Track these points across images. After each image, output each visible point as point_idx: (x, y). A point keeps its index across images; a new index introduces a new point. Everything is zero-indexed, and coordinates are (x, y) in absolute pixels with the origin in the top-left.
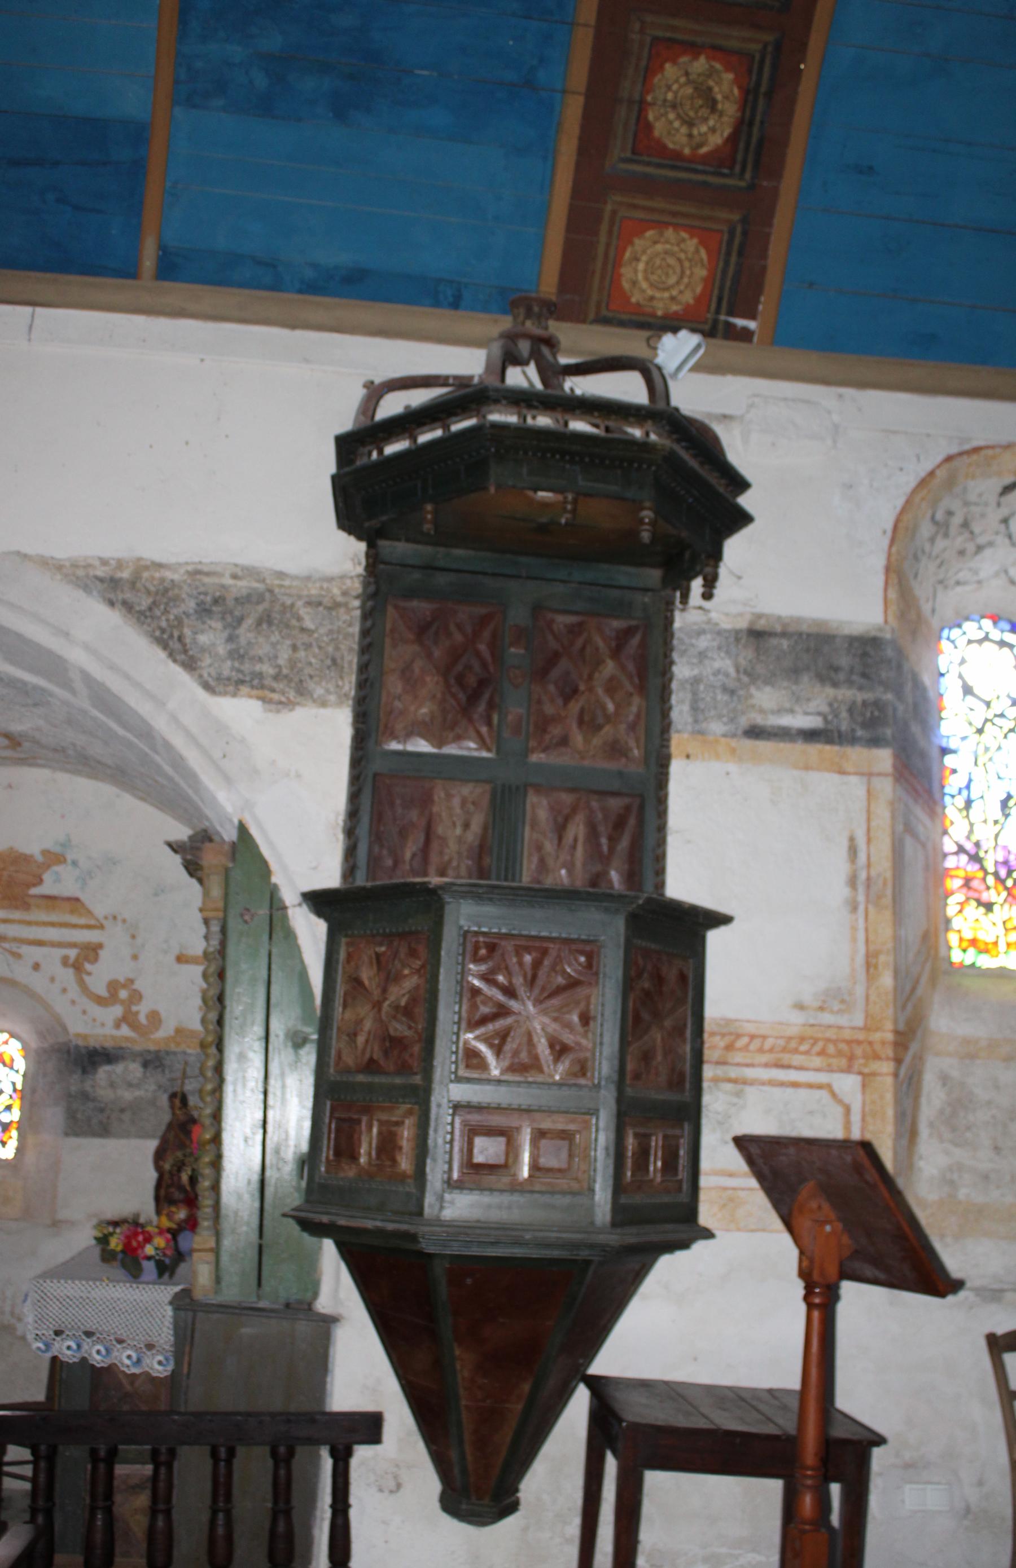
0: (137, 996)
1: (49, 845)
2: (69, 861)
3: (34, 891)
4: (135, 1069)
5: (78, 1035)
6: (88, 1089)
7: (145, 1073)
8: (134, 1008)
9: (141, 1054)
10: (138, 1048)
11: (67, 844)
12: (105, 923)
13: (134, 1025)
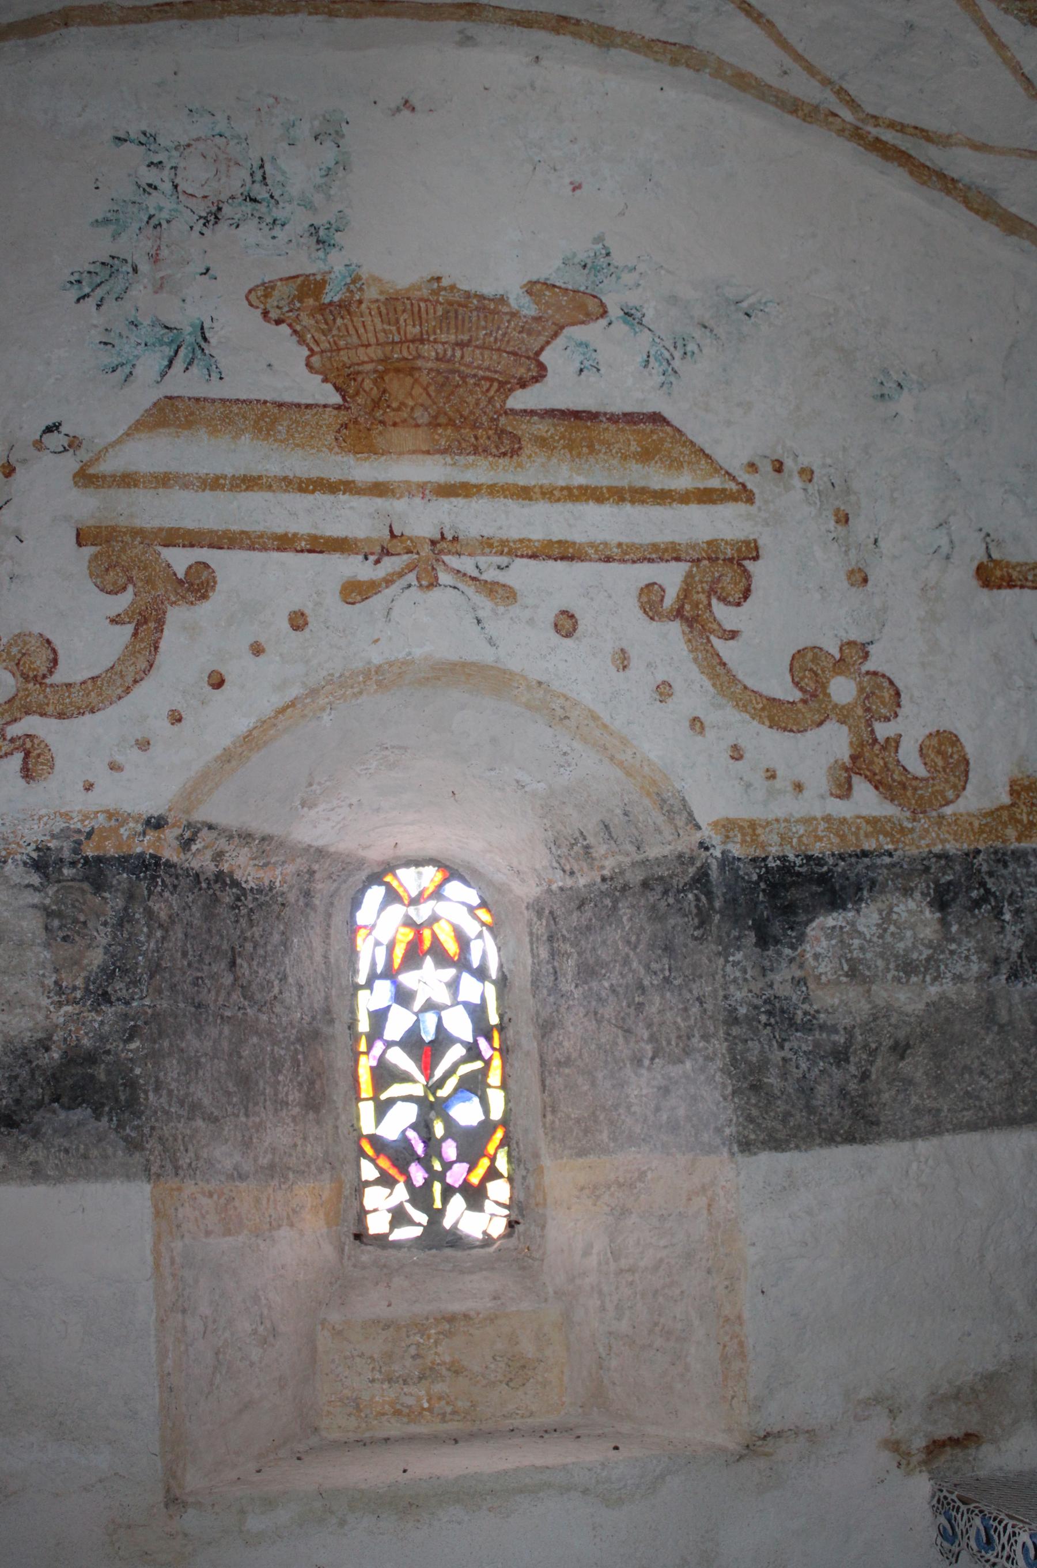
0: (883, 695)
1: (548, 268)
2: (614, 312)
3: (520, 400)
4: (914, 916)
5: (727, 827)
6: (783, 990)
7: (944, 923)
8: (883, 730)
9: (922, 866)
10: (913, 848)
11: (599, 263)
12: (751, 481)
13: (891, 784)
